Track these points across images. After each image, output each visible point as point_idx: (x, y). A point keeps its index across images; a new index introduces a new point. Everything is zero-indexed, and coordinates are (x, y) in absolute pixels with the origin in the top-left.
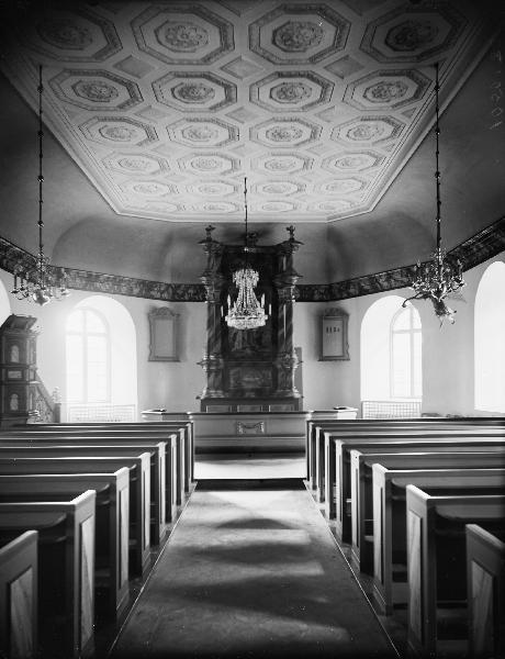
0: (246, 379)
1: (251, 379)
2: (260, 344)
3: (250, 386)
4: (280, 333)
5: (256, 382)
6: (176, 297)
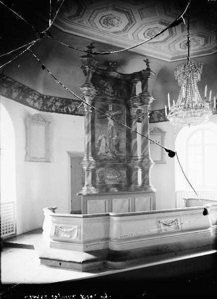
0: (108, 177)
1: (112, 177)
2: (118, 150)
3: (112, 183)
4: (133, 142)
5: (116, 179)
6: (45, 107)
